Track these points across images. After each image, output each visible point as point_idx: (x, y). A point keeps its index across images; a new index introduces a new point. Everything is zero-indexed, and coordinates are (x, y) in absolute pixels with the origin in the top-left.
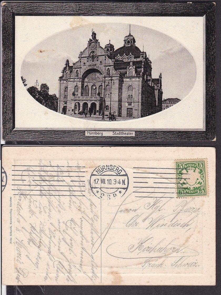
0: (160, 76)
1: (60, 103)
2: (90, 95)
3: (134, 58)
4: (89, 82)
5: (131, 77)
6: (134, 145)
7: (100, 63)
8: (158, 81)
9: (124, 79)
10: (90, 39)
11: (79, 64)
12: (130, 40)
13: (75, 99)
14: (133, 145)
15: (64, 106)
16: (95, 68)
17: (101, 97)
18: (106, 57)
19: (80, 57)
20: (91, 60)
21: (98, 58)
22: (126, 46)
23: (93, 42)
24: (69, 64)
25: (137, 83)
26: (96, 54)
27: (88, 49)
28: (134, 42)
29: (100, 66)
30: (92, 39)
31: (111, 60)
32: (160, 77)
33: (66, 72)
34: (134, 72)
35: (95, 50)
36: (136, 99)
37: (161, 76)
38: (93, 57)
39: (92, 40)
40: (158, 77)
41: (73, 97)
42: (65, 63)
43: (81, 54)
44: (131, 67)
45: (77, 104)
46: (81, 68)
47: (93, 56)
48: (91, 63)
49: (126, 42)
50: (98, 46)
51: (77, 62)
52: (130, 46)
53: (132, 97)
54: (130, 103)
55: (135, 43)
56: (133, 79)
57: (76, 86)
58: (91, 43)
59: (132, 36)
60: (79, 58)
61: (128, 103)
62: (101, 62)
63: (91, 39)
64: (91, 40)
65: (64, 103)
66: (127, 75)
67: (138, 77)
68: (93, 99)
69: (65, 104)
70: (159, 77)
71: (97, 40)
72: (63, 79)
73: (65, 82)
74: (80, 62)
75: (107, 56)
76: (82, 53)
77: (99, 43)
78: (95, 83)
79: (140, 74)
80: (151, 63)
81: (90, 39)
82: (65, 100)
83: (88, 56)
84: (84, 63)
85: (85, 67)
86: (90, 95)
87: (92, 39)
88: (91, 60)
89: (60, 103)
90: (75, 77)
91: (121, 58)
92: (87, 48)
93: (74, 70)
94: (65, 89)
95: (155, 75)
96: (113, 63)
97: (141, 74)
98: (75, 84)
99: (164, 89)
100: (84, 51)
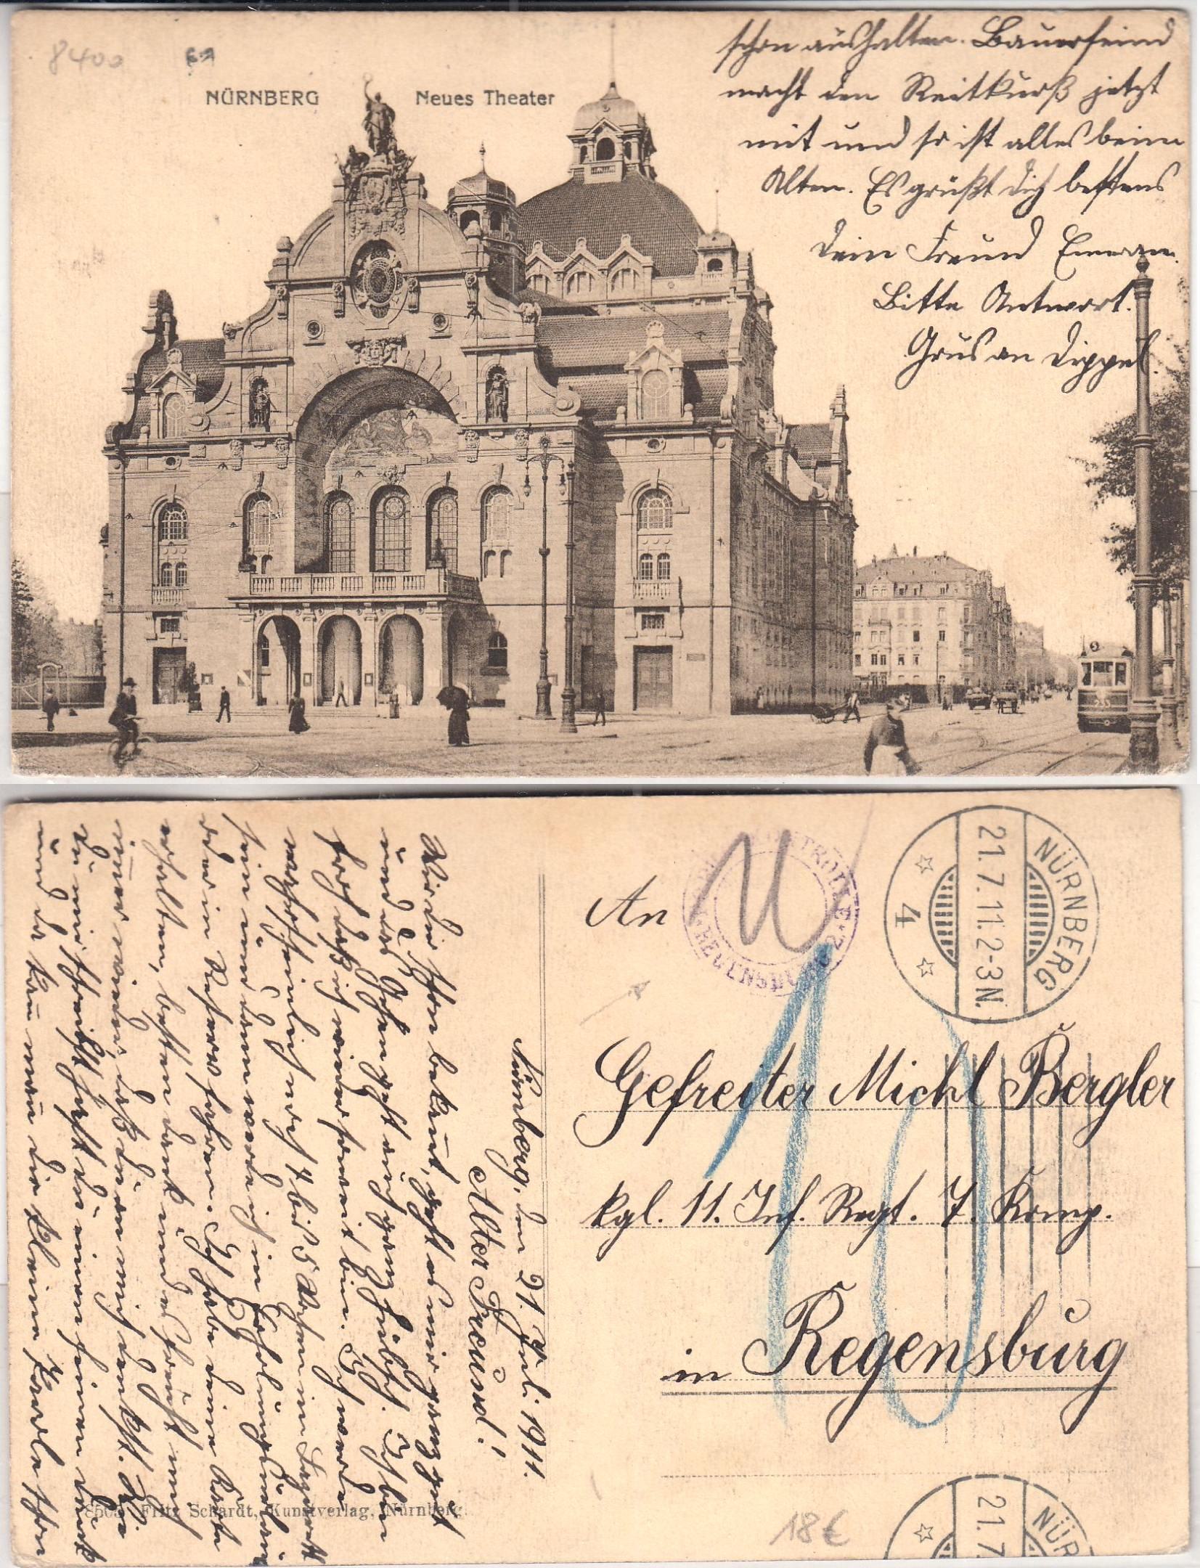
0: (839, 409)
2: (655, 575)
3: (656, 274)
4: (356, 471)
5: (654, 434)
9: (609, 443)
10: (352, 149)
13: (257, 593)
15: (159, 644)
16: (400, 359)
17: (454, 579)
18: (475, 287)
19: (286, 286)
20: (363, 305)
21: (417, 290)
22: (590, 179)
23: (378, 175)
24: (173, 322)
26: (399, 265)
27: (337, 224)
28: (648, 147)
30: (370, 153)
31: (512, 306)
33: (167, 389)
35: (391, 236)
36: (696, 586)
37: (844, 406)
38: (374, 277)
39: (365, 158)
40: (821, 415)
41: (241, 585)
42: (145, 316)
43: (285, 254)
44: (654, 355)
45: (271, 633)
46: (290, 362)
47: (378, 273)
48: (361, 323)
49: (584, 151)
50: (412, 201)
51: (254, 321)
52: (615, 176)
53: (665, 572)
54: (169, 617)
55: (653, 156)
56: (675, 445)
58: (358, 180)
59: (629, 103)
60: (271, 285)
61: (639, 615)
62: (439, 319)
63: (363, 146)
64: (357, 159)
65: (152, 627)
66: (626, 413)
67: (703, 426)
68: (276, 592)
69: (168, 635)
71: (402, 158)
72: (142, 440)
73: (158, 464)
74: (284, 316)
75: (482, 280)
77: (421, 180)
78: (401, 470)
80: (770, 306)
81: (352, 149)
82: (165, 600)
83: (340, 273)
84: (313, 327)
85: (318, 354)
86: (655, 575)
87: (370, 153)
88: (363, 305)
90: (247, 430)
91: (558, 273)
92: (325, 219)
94: (162, 516)
95: (797, 399)
96: (530, 327)
100: (308, 238)
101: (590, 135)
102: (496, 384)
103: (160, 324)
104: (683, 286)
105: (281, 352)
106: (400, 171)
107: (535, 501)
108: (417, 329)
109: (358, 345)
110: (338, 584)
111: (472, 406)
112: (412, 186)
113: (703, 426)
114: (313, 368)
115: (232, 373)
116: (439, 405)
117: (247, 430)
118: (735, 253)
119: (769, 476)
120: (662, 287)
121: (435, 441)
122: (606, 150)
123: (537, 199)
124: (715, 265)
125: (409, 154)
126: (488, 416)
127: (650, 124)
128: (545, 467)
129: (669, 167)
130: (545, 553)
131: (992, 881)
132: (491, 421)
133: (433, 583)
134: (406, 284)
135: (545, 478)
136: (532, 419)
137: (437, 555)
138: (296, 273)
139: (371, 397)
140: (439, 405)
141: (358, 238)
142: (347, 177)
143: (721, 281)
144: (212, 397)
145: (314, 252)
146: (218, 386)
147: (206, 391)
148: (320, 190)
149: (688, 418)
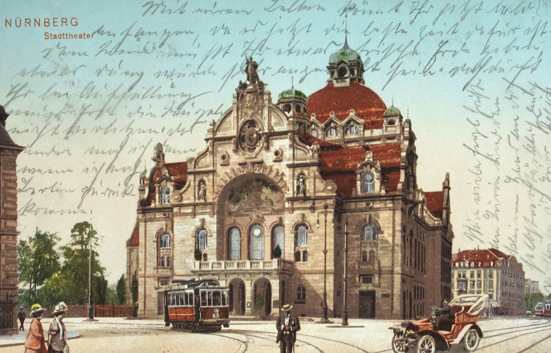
1: (145, 283)
6: (284, 289)
7: (274, 157)
8: (439, 203)
11: (208, 159)
12: (347, 67)
14: (284, 289)
15: (160, 290)
17: (283, 262)
22: (336, 85)
25: (389, 221)
27: (234, 114)
28: (361, 70)
29: (276, 166)
30: (248, 83)
32: (447, 187)
34: (377, 184)
40: (440, 189)
57: (202, 228)
60: (207, 140)
64: (243, 86)
67: (390, 196)
70: (442, 187)
71: (262, 85)
72: (153, 205)
76: (216, 127)
77: (269, 94)
79: (395, 189)
81: (240, 82)
85: (228, 169)
87: (248, 83)
89: (145, 283)
93: (191, 178)
95: (427, 181)
97: (400, 186)
98: (197, 222)
99: (458, 220)
100: (222, 121)
101: (336, 66)
102: (301, 180)
103: (158, 156)
104: (377, 132)
105: (211, 168)
106: (260, 90)
107: (322, 231)
108: (268, 157)
109: (243, 165)
110: (236, 265)
111: (291, 189)
112: (266, 97)
113: (390, 196)
114: (224, 175)
115: (191, 178)
116: (275, 188)
117: (197, 201)
118: (401, 118)
119: (416, 216)
120: (368, 133)
121: (275, 204)
122: (342, 73)
123: (313, 95)
124: (392, 123)
125: (265, 82)
126: (298, 193)
127: (453, 195)
128: (326, 216)
129: (372, 81)
130: (325, 252)
131: (542, 89)
132: (299, 195)
133: (274, 264)
134: (263, 139)
135: (326, 221)
136: (318, 194)
137: (276, 252)
138: (219, 135)
139: (250, 186)
140: (275, 188)
141: (243, 119)
142: (238, 94)
143: (395, 130)
144: (182, 187)
145: (224, 125)
146: (184, 183)
147: (180, 185)
148: (227, 100)
149: (383, 192)
